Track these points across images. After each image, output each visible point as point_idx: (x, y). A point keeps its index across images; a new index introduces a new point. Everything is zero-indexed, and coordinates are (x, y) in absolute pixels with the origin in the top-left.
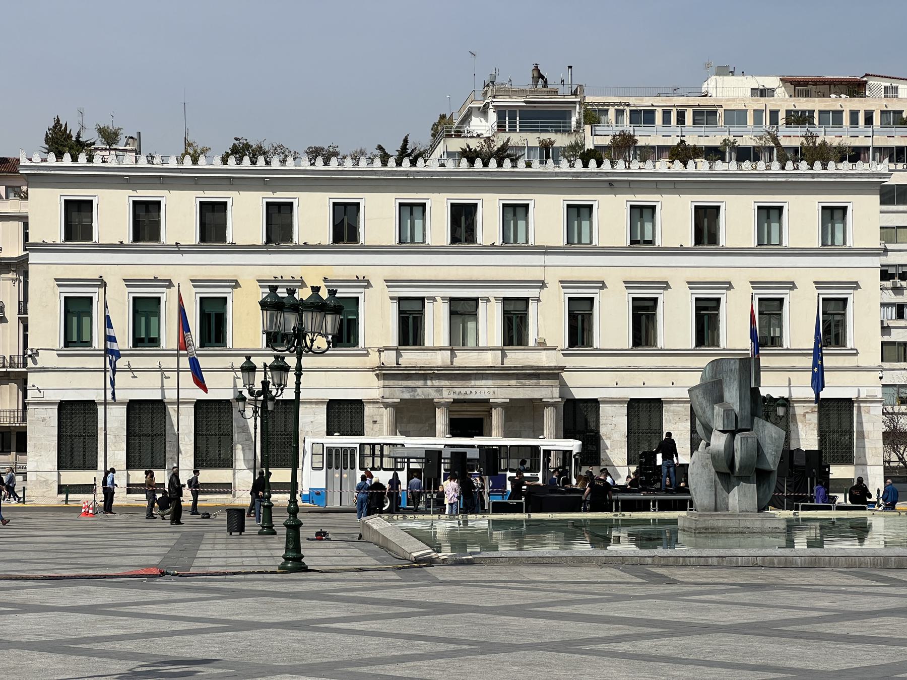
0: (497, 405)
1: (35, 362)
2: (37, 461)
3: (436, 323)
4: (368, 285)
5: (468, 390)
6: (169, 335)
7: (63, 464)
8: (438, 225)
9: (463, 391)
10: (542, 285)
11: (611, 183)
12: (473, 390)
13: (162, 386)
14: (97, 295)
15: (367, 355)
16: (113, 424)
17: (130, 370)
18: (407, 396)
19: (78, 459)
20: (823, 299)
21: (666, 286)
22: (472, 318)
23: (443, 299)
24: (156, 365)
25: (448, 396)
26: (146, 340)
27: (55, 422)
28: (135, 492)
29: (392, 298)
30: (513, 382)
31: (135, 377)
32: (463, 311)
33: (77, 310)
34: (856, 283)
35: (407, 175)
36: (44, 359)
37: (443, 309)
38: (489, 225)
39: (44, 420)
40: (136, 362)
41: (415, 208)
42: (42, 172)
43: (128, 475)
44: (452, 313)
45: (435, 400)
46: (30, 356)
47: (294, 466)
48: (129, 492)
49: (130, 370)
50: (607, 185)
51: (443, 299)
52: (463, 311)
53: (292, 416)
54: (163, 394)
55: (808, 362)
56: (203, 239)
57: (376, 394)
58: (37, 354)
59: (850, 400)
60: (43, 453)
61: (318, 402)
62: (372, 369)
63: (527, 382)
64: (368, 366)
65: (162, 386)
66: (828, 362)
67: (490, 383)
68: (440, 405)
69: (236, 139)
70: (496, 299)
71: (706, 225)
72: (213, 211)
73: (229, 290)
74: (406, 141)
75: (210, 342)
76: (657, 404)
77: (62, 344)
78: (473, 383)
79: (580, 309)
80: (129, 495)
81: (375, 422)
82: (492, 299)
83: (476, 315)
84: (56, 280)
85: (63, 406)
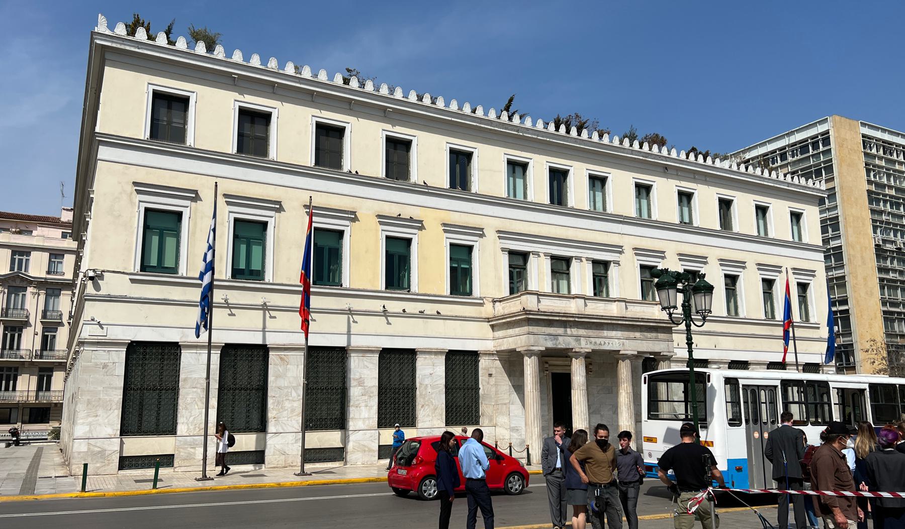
0: (625, 357)
1: (97, 287)
2: (90, 424)
3: (539, 273)
4: (355, 219)
5: (602, 341)
6: (190, 263)
7: (130, 426)
8: (538, 187)
9: (598, 341)
10: (619, 249)
11: (666, 167)
12: (607, 341)
13: (264, 327)
14: (188, 210)
15: (481, 305)
16: (197, 374)
17: (227, 305)
18: (550, 344)
19: (149, 418)
20: (315, 228)
21: (420, 225)
22: (259, 244)
23: (546, 255)
24: (260, 301)
25: (585, 346)
26: (246, 272)
27: (121, 370)
28: (130, 467)
29: (503, 250)
30: (638, 335)
31: (232, 315)
32: (561, 267)
33: (161, 225)
34: (279, 203)
35: (518, 131)
36: (110, 285)
37: (546, 264)
38: (578, 191)
39: (105, 366)
40: (236, 297)
41: (460, 157)
42: (128, 48)
43: (122, 443)
44: (553, 272)
45: (577, 350)
46: (91, 278)
47: (261, 427)
48: (121, 467)
49: (227, 305)
50: (661, 170)
51: (546, 255)
52: (561, 267)
53: (257, 365)
54: (264, 338)
55: (296, 301)
56: (241, 149)
57: (490, 346)
58: (101, 277)
59: (342, 349)
60: (100, 412)
61: (437, 353)
62: (488, 320)
63: (649, 335)
64: (484, 316)
65: (264, 327)
66: (315, 302)
67: (619, 334)
68: (577, 355)
69: (349, 70)
70: (588, 259)
71: (253, 129)
72: (327, 135)
73: (347, 223)
74: (511, 100)
75: (322, 280)
76: (410, 354)
77: (138, 267)
78: (606, 333)
79: (399, 249)
80: (121, 472)
81: (490, 375)
82: (584, 260)
83: (568, 274)
84: (135, 184)
85: (135, 349)
